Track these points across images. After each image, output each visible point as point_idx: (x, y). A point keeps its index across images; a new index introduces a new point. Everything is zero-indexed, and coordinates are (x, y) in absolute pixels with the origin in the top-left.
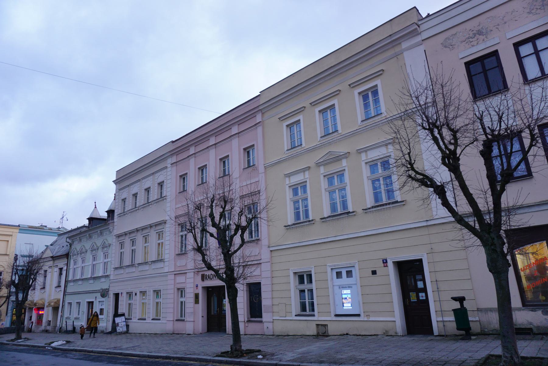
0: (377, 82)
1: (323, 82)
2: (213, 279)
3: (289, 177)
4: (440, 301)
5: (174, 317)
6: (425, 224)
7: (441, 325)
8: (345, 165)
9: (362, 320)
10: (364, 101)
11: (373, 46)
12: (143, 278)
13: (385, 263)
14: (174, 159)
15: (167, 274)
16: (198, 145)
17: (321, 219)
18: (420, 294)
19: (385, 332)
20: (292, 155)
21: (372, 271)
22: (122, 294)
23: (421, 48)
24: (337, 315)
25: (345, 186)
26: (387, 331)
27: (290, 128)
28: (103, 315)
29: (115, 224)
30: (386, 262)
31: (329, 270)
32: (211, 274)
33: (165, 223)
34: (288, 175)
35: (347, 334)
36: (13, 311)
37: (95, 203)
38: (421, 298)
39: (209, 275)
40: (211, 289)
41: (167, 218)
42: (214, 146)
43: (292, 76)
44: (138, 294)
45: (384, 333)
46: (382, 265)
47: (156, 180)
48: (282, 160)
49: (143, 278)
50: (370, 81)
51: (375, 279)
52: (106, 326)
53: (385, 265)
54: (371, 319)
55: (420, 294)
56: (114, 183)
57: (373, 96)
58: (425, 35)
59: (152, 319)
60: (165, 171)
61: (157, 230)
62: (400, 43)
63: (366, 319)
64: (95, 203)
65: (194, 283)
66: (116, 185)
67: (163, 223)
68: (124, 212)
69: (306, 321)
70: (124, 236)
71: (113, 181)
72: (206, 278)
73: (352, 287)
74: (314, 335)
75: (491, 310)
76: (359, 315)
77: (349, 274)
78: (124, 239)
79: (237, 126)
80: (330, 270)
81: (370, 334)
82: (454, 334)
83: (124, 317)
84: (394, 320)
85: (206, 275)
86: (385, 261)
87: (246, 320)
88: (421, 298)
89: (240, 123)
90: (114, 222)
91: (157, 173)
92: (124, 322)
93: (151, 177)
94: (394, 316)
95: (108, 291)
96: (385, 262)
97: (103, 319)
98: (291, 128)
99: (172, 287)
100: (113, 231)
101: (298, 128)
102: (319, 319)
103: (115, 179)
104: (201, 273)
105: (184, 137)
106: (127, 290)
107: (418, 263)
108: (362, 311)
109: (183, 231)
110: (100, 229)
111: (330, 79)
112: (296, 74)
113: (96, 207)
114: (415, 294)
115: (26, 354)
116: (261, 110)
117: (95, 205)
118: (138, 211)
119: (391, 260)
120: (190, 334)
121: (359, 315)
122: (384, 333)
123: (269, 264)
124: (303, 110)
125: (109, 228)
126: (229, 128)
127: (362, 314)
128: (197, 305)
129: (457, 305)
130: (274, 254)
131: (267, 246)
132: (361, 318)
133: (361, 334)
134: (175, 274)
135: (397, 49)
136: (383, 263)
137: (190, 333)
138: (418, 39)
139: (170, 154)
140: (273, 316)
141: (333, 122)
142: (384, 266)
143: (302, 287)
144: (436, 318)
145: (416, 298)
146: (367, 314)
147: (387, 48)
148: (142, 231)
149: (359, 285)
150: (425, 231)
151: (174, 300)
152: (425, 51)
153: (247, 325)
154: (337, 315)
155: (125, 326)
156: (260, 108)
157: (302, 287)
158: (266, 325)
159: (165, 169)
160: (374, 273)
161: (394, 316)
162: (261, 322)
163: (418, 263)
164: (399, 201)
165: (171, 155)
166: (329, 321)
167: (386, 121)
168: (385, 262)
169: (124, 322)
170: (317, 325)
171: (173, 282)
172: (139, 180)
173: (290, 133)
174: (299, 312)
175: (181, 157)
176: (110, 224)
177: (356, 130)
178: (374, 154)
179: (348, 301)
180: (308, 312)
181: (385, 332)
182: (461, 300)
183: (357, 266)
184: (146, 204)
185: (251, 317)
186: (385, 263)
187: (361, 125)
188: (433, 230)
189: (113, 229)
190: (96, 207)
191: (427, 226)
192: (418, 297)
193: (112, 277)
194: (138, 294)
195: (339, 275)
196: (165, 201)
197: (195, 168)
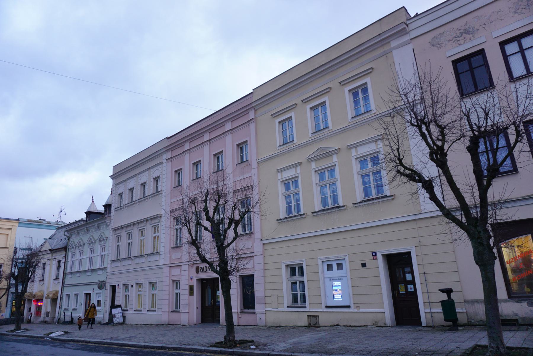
0: (367, 80)
1: (314, 80)
2: (207, 271)
4: (428, 293)
5: (169, 309)
6: (413, 218)
7: (429, 316)
9: (352, 311)
10: (354, 98)
11: (363, 45)
12: (139, 271)
13: (374, 255)
14: (169, 155)
15: (162, 266)
16: (193, 141)
18: (409, 286)
19: (374, 323)
20: (284, 151)
21: (362, 264)
25: (336, 181)
26: (376, 322)
27: (282, 124)
28: (100, 306)
29: (112, 218)
30: (376, 255)
32: (205, 267)
33: (161, 217)
34: (281, 171)
35: (338, 325)
37: (93, 197)
38: (409, 290)
39: (203, 267)
40: (205, 281)
42: (209, 142)
43: (284, 74)
44: (134, 286)
45: (374, 324)
46: (372, 258)
47: (152, 175)
48: (274, 156)
49: (139, 271)
50: (360, 79)
51: (365, 272)
52: (103, 317)
53: (375, 258)
54: (361, 310)
55: (409, 286)
56: (111, 178)
57: (363, 94)
58: (413, 34)
59: (148, 311)
60: (161, 166)
61: (153, 224)
62: (389, 42)
63: (356, 310)
64: (93, 197)
65: (188, 275)
66: (113, 180)
67: (158, 217)
68: (121, 206)
69: (298, 312)
71: (110, 177)
72: (200, 270)
73: (342, 279)
76: (349, 307)
78: (121, 233)
81: (360, 325)
82: (441, 325)
84: (383, 311)
85: (200, 267)
86: (374, 254)
88: (409, 290)
89: (233, 120)
90: (111, 216)
91: (152, 168)
92: (121, 313)
93: (147, 172)
94: (383, 308)
95: (105, 283)
96: (374, 255)
97: (101, 311)
98: (283, 124)
99: (168, 279)
100: (110, 224)
101: (290, 125)
102: (310, 311)
103: (112, 174)
105: (179, 133)
106: (124, 282)
107: (406, 256)
109: (178, 225)
110: (97, 223)
112: (288, 72)
113: (93, 202)
114: (404, 286)
115: (25, 344)
116: (253, 107)
117: (93, 200)
118: (134, 205)
119: (380, 253)
120: (185, 325)
121: (349, 307)
122: (374, 324)
123: (262, 256)
124: (295, 107)
125: (106, 222)
126: (223, 125)
127: (352, 306)
128: (191, 297)
130: (267, 247)
131: (260, 240)
132: (351, 309)
133: (352, 325)
134: (170, 267)
136: (373, 255)
137: (184, 324)
138: (407, 38)
139: (165, 150)
140: (265, 307)
141: (324, 118)
142: (374, 259)
143: (294, 279)
144: (425, 310)
145: (404, 290)
146: (357, 305)
147: (377, 47)
148: (138, 225)
150: (413, 225)
151: (169, 292)
152: (413, 49)
153: (240, 316)
155: (122, 317)
156: (253, 105)
157: (294, 279)
158: (258, 316)
159: (160, 164)
162: (254, 313)
163: (406, 256)
165: (166, 150)
166: (320, 313)
167: (376, 118)
168: (374, 255)
169: (121, 313)
170: (309, 316)
171: (168, 274)
172: (135, 176)
173: (283, 130)
174: (291, 303)
175: (176, 152)
176: (107, 218)
177: (347, 126)
178: (364, 150)
179: (339, 293)
180: (299, 304)
181: (374, 323)
183: (347, 259)
184: (142, 198)
186: (374, 255)
187: (351, 122)
188: (421, 224)
189: (110, 223)
190: (93, 202)
191: (415, 220)
192: (406, 288)
193: (109, 270)
194: (134, 286)
195: (330, 267)
196: (160, 195)
197: (190, 163)
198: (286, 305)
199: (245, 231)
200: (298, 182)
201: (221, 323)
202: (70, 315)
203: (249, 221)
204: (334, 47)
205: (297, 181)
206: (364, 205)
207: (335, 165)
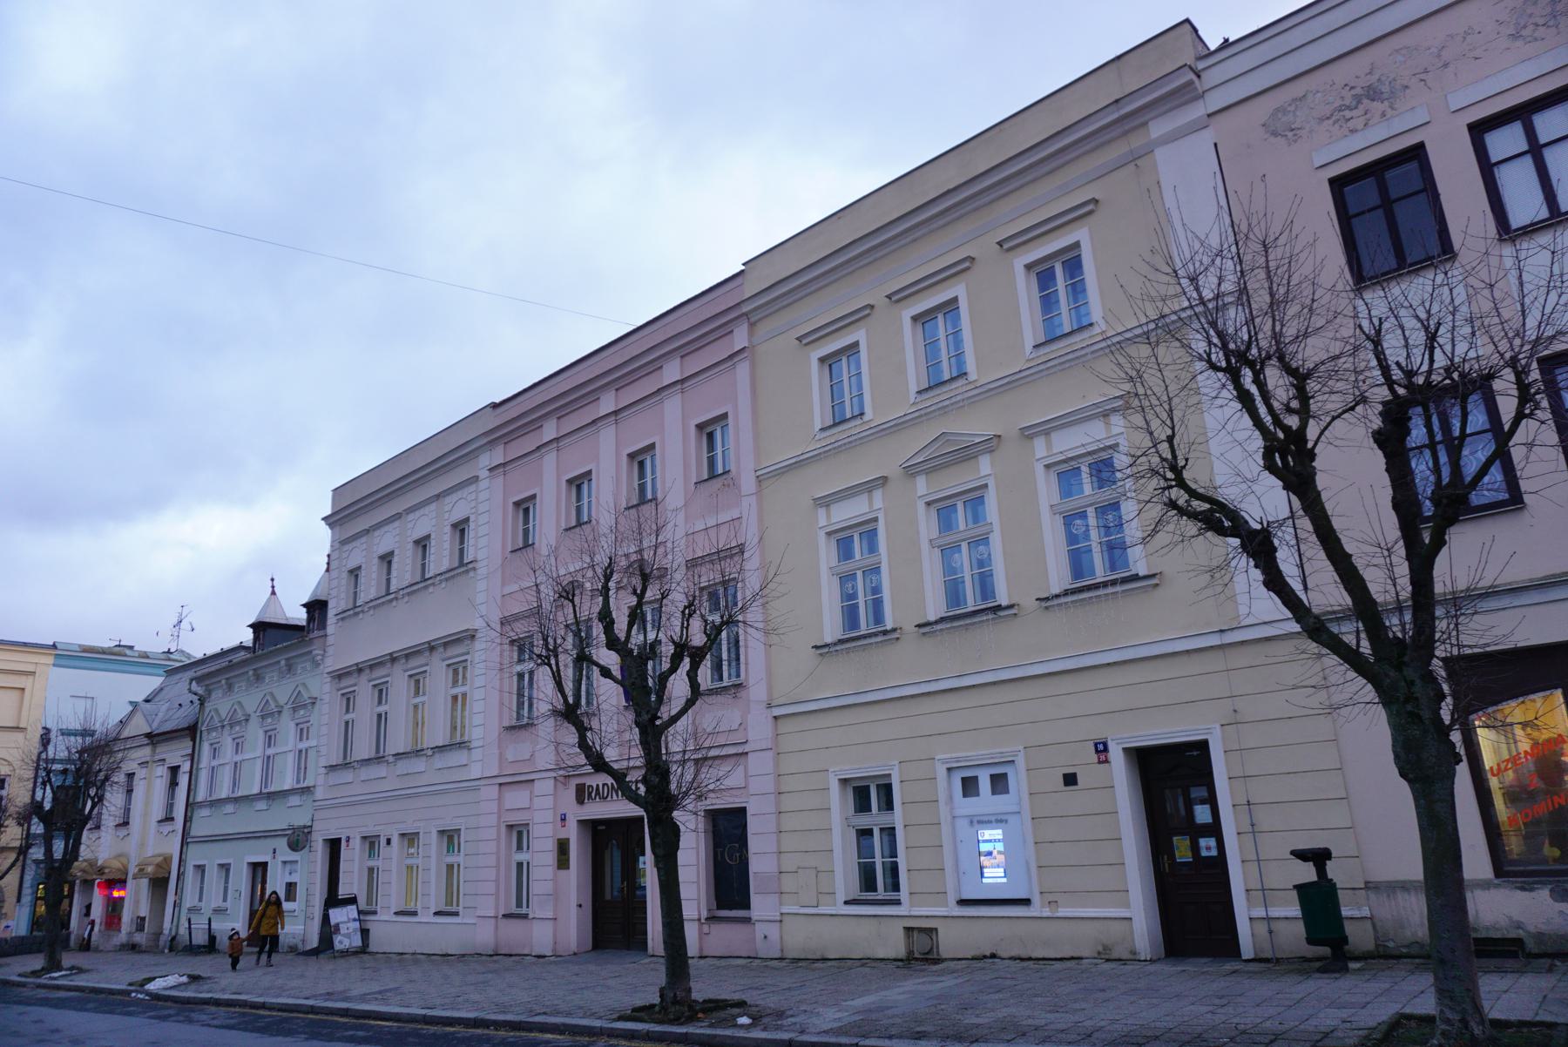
0: (1080, 234)
1: (924, 235)
2: (609, 798)
3: (828, 506)
4: (1258, 860)
5: (497, 908)
6: (1215, 640)
7: (1262, 929)
8: (988, 471)
9: (1035, 914)
10: (1042, 288)
11: (1066, 132)
12: (409, 796)
13: (1101, 751)
14: (497, 456)
15: (477, 783)
16: (567, 414)
17: (919, 626)
18: (1203, 842)
19: (1101, 949)
20: (836, 445)
21: (1065, 776)
22: (348, 840)
23: (1206, 139)
24: (963, 902)
25: (988, 533)
26: (1106, 948)
27: (830, 365)
28: (295, 901)
29: (330, 640)
30: (1106, 749)
31: (941, 771)
32: (604, 785)
33: (473, 637)
34: (825, 502)
35: (993, 956)
36: (38, 889)
37: (272, 580)
38: (1204, 853)
39: (598, 785)
40: (604, 827)
41: (478, 624)
42: (613, 418)
43: (835, 217)
44: (395, 840)
45: (1099, 953)
46: (1094, 758)
47: (447, 515)
48: (807, 459)
49: (409, 796)
50: (1058, 233)
51: (1073, 799)
52: (302, 932)
53: (1103, 757)
54: (1063, 912)
55: (1203, 842)
56: (327, 524)
57: (1067, 276)
58: (1215, 101)
59: (436, 914)
60: (472, 488)
61: (449, 658)
62: (1145, 124)
63: (1047, 912)
64: (272, 580)
65: (554, 808)
66: (331, 528)
67: (465, 638)
68: (356, 607)
69: (876, 919)
70: (355, 675)
71: (323, 519)
72: (590, 794)
73: (1006, 821)
74: (900, 957)
75: (1405, 886)
76: (1026, 902)
77: (999, 783)
78: (355, 685)
79: (678, 360)
80: (945, 771)
81: (1058, 957)
82: (1299, 955)
83: (354, 907)
84: (1127, 915)
85: (589, 786)
86: (1101, 747)
87: (704, 914)
88: (1204, 853)
89: (685, 352)
90: (326, 636)
91: (448, 495)
92: (355, 920)
93: (433, 506)
94: (1127, 905)
95: (310, 833)
96: (1102, 749)
97: (296, 914)
98: (833, 366)
99: (493, 820)
100: (322, 660)
101: (853, 367)
102: (913, 913)
103: (328, 512)
104: (574, 782)
105: (525, 391)
106: (364, 829)
107: (1195, 753)
108: (1036, 891)
109: (524, 660)
110: (286, 656)
111: (944, 226)
112: (846, 211)
113: (273, 593)
114: (1188, 842)
116: (746, 314)
117: (273, 587)
118: (394, 603)
119: (1118, 744)
120: (544, 957)
121: (1026, 902)
122: (1099, 953)
123: (770, 754)
124: (868, 315)
125: (311, 652)
126: (655, 366)
127: (1036, 899)
128: (563, 873)
129: (1307, 873)
130: (785, 726)
131: (765, 705)
132: (1032, 909)
133: (1034, 955)
134: (500, 784)
135: (1136, 141)
136: (1097, 751)
137: (542, 954)
138: (1197, 111)
139: (485, 441)
140: (781, 904)
141: (952, 348)
142: (1100, 762)
143: (864, 821)
144: (1249, 910)
145: (1190, 854)
146: (1051, 897)
147: (1108, 137)
148: (407, 660)
149: (1027, 816)
150: (1216, 662)
152: (1216, 145)
153: (706, 928)
154: (963, 902)
155: (359, 933)
156: (745, 308)
157: (864, 821)
158: (760, 930)
159: (471, 484)
160: (1070, 780)
161: (1127, 905)
162: (747, 920)
163: (1195, 753)
164: (1141, 574)
165: (490, 442)
166: (942, 919)
167: (1105, 348)
168: (1102, 749)
170: (908, 930)
171: (494, 807)
172: (398, 516)
173: (831, 381)
174: (855, 892)
175: (518, 448)
176: (316, 641)
177: (1020, 371)
178: (1071, 442)
179: (996, 861)
180: (881, 893)
181: (1101, 949)
182: (1319, 857)
183: (1021, 762)
184: (418, 583)
185: (719, 907)
186: (1101, 751)
187: (1033, 359)
188: (1240, 658)
189: (323, 655)
190: (273, 593)
191: (1221, 647)
192: (1195, 848)
193: (319, 793)
194: (395, 840)
195: (970, 786)
196: (471, 574)
197: (558, 479)
198: (841, 897)
199: (721, 679)
200: (876, 535)
201: (650, 951)
202: (207, 927)
203: (733, 650)
204: (983, 137)
205: (874, 532)
206: (1072, 602)
207: (986, 486)
